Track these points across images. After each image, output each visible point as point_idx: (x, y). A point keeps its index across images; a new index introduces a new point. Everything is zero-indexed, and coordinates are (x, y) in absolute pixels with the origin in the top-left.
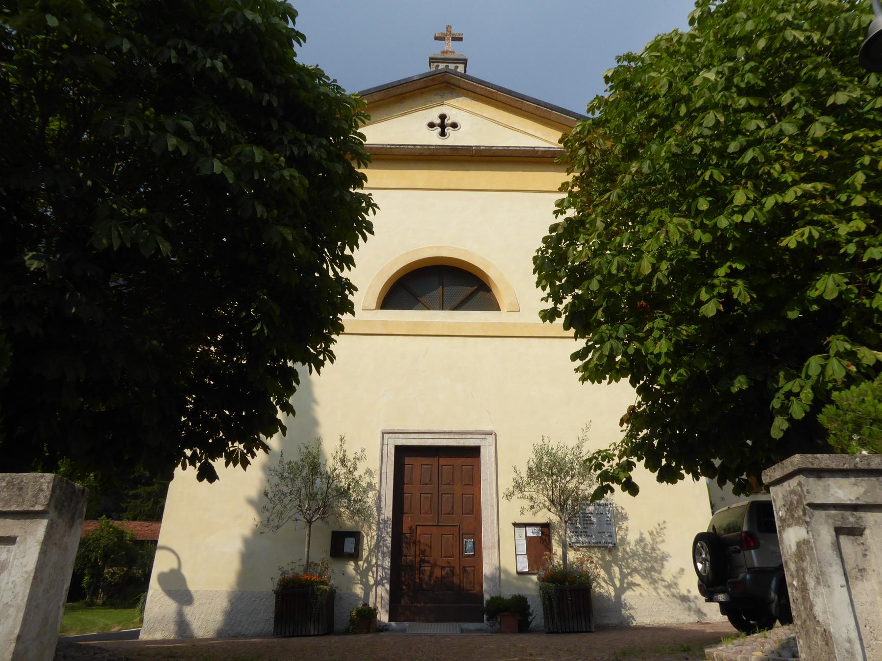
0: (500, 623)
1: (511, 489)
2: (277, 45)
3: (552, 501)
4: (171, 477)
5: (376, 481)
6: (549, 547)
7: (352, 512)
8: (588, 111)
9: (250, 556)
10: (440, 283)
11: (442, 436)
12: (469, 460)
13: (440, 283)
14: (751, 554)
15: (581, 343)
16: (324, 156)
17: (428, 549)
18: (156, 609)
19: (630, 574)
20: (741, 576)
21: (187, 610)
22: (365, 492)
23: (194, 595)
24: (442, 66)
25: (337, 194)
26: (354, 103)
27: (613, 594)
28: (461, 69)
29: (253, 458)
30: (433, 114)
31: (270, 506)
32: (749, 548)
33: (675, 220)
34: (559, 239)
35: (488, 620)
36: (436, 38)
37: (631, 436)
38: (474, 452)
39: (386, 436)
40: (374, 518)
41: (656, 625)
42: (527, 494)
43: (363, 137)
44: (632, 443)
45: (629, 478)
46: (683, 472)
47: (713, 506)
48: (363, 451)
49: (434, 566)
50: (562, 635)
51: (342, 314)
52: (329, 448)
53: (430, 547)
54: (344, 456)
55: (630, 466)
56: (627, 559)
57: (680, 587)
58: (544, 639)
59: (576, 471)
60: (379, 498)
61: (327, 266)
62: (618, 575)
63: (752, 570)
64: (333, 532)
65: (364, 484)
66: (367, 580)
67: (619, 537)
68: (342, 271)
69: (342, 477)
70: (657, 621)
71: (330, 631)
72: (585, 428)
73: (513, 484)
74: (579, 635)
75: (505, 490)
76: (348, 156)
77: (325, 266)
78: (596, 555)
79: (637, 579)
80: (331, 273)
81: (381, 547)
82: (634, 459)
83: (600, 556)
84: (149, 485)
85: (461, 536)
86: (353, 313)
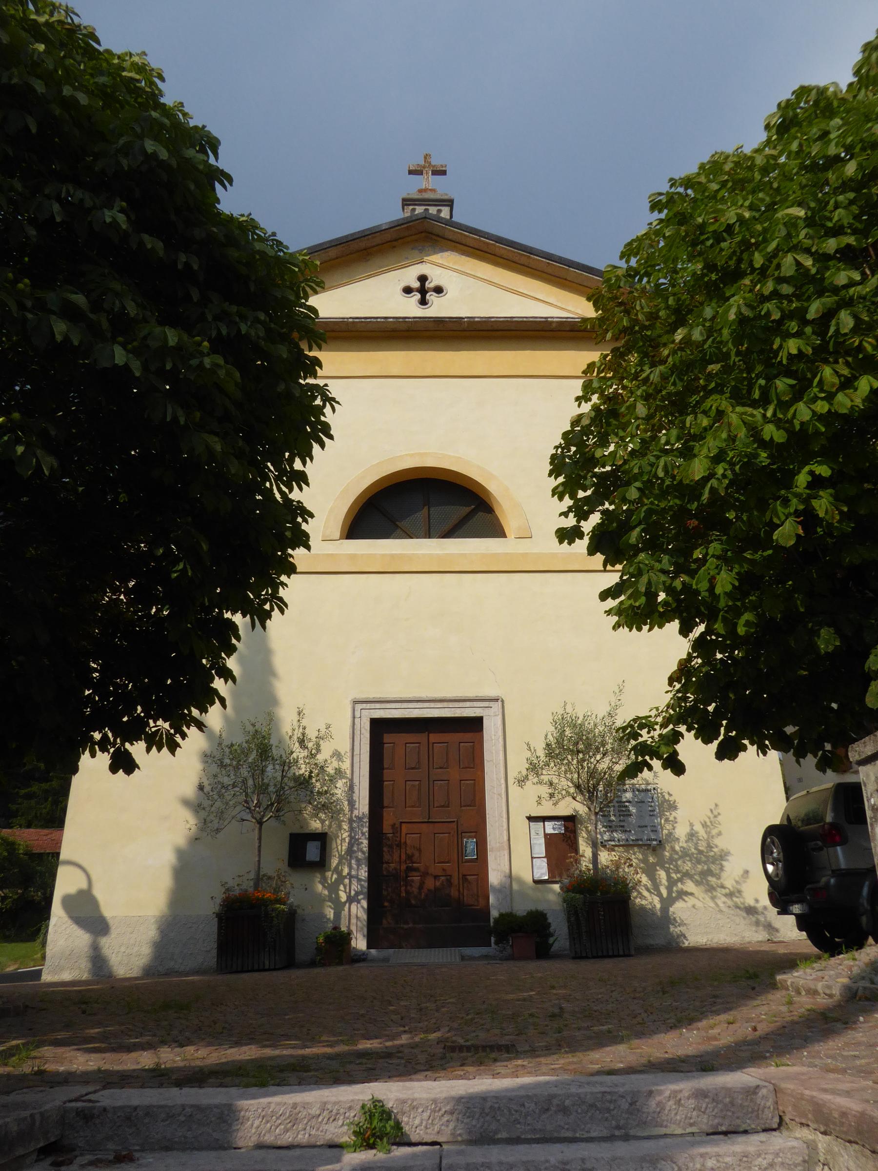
0: (512, 946)
1: (524, 773)
2: (192, 187)
3: (578, 787)
4: (75, 770)
5: (346, 766)
6: (575, 847)
7: (316, 808)
8: (621, 258)
9: (185, 869)
10: (426, 502)
11: (432, 705)
12: (468, 736)
13: (426, 502)
14: (836, 851)
15: (612, 579)
16: (262, 334)
17: (417, 854)
18: (61, 942)
19: (680, 880)
20: (824, 880)
21: (104, 941)
22: (332, 780)
23: (111, 922)
24: (419, 210)
25: (281, 387)
26: (302, 265)
27: (658, 906)
28: (445, 213)
29: (183, 739)
30: (410, 276)
31: (207, 803)
32: (835, 844)
33: (739, 409)
34: (586, 431)
35: (496, 943)
36: (411, 172)
37: (679, 700)
38: (475, 725)
39: (359, 707)
40: (345, 815)
41: (715, 945)
42: (545, 778)
43: (314, 310)
44: (680, 707)
45: (675, 753)
46: (746, 742)
47: (788, 790)
48: (328, 727)
49: (425, 874)
50: (592, 961)
51: (293, 549)
52: (287, 721)
53: (420, 850)
54: (303, 734)
55: (676, 737)
56: (676, 861)
57: (744, 894)
58: (570, 966)
59: (609, 747)
60: (351, 788)
61: (271, 485)
62: (664, 881)
63: (838, 873)
64: (291, 835)
65: (330, 770)
66: (338, 897)
67: (665, 832)
68: (291, 490)
69: (301, 762)
70: (715, 941)
71: (290, 963)
72: (617, 691)
73: (527, 766)
74: (615, 960)
75: (516, 774)
76: (295, 335)
77: (268, 485)
78: (636, 856)
79: (689, 886)
80: (278, 496)
81: (355, 852)
82: (682, 728)
83: (641, 857)
84: (47, 780)
85: (460, 834)
86: (308, 548)
